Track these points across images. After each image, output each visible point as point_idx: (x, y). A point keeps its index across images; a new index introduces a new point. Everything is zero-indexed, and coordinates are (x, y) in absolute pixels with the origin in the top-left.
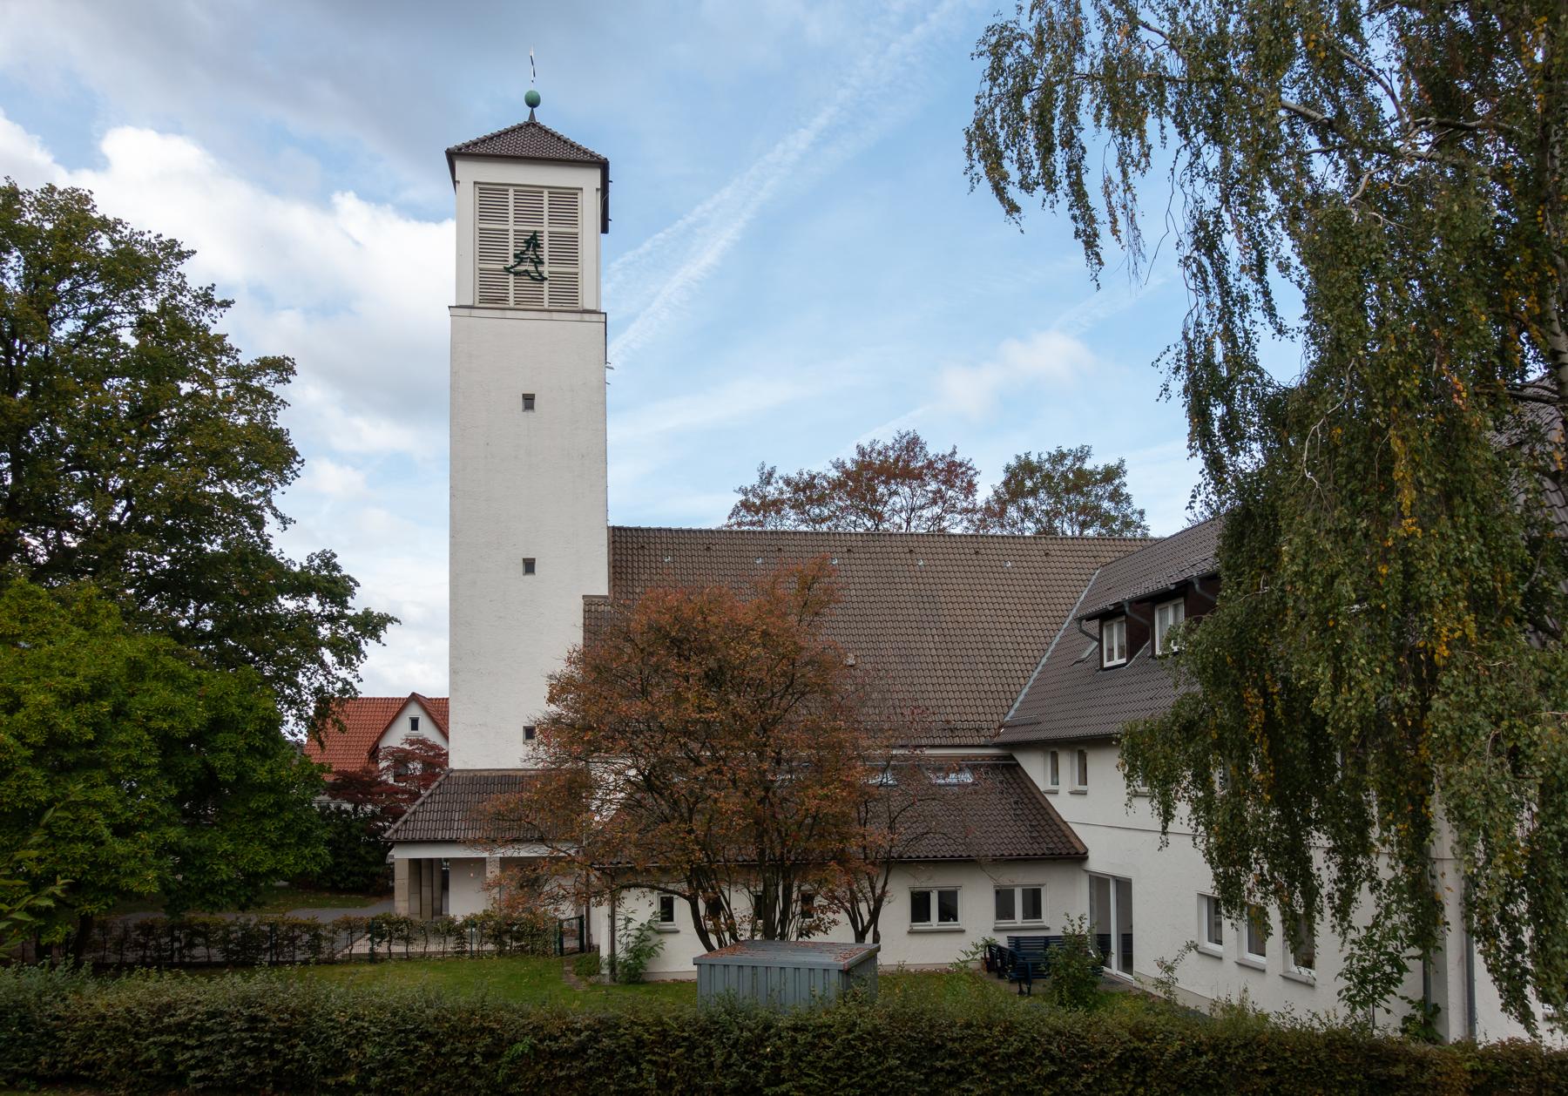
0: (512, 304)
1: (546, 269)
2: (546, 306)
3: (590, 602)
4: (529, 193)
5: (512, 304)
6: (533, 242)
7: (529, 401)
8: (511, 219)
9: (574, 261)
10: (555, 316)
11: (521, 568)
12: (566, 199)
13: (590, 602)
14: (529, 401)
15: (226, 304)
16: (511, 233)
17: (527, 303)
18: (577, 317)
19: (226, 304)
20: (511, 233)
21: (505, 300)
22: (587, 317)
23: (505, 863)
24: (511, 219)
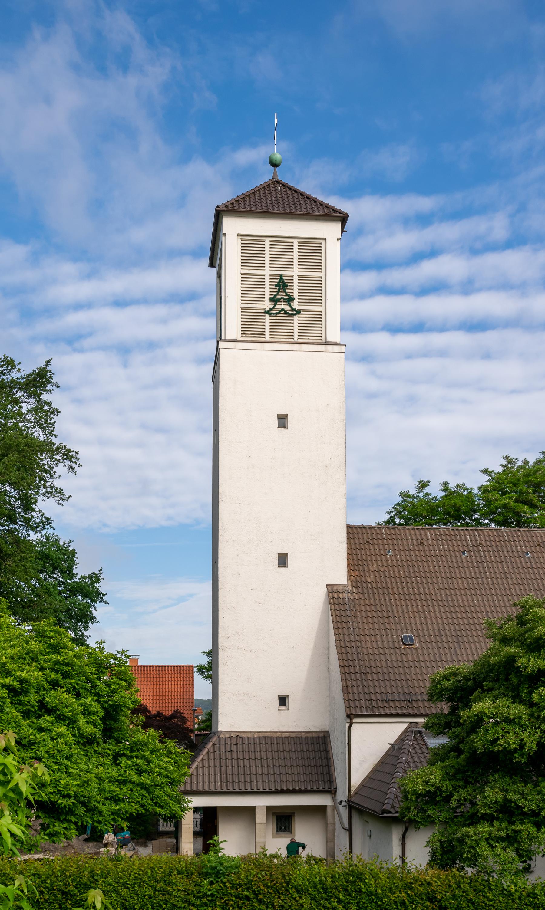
0: (268, 338)
1: (296, 305)
2: (296, 339)
3: (333, 591)
4: (282, 243)
5: (268, 338)
6: (281, 284)
7: (282, 420)
8: (268, 265)
9: (318, 300)
10: (304, 347)
11: (291, 560)
12: (313, 248)
13: (333, 591)
14: (282, 420)
15: (106, 603)
16: (268, 278)
17: (282, 336)
18: (322, 348)
19: (106, 603)
20: (268, 278)
21: (262, 334)
22: (330, 348)
23: (270, 809)
24: (268, 265)
